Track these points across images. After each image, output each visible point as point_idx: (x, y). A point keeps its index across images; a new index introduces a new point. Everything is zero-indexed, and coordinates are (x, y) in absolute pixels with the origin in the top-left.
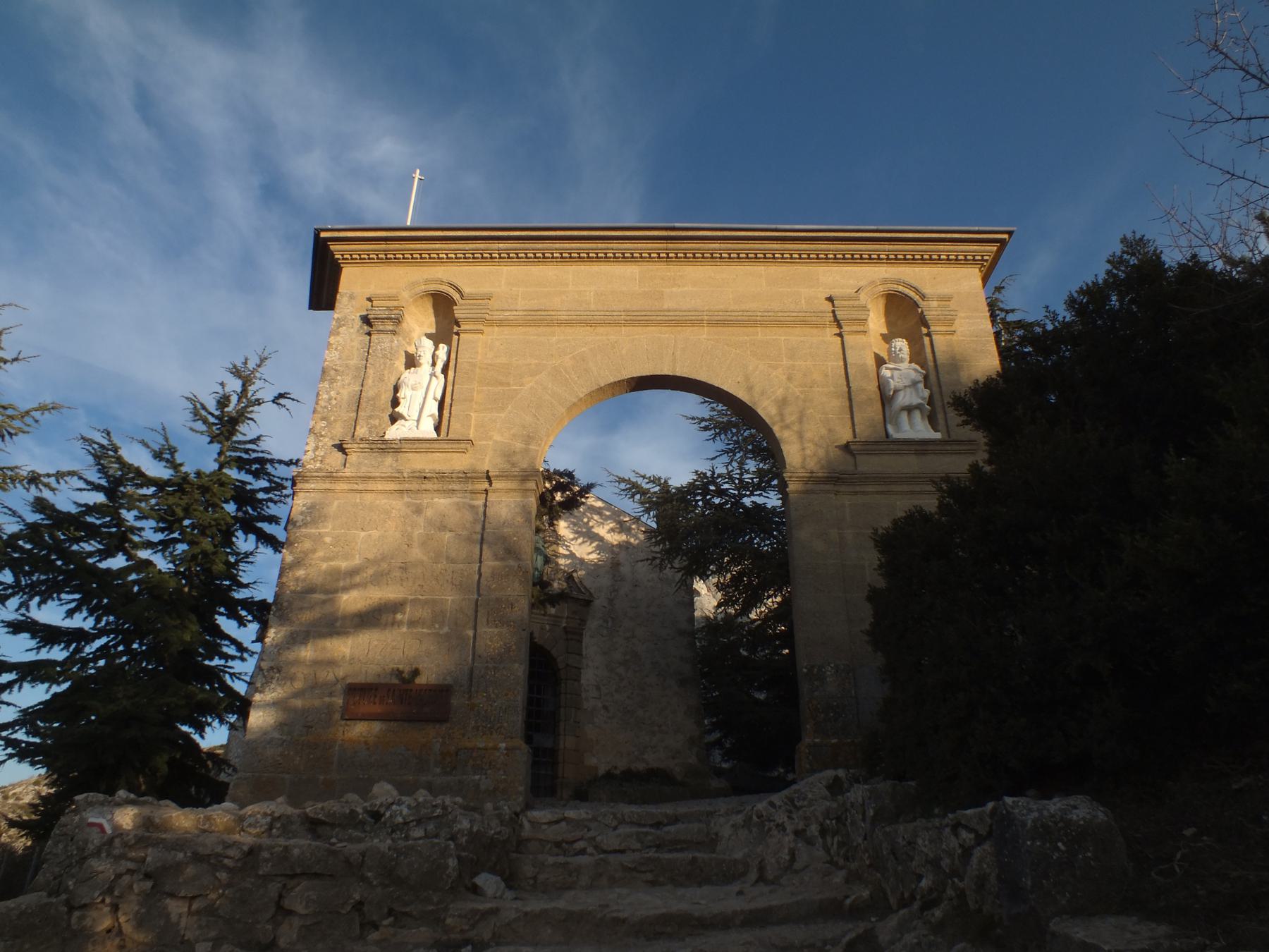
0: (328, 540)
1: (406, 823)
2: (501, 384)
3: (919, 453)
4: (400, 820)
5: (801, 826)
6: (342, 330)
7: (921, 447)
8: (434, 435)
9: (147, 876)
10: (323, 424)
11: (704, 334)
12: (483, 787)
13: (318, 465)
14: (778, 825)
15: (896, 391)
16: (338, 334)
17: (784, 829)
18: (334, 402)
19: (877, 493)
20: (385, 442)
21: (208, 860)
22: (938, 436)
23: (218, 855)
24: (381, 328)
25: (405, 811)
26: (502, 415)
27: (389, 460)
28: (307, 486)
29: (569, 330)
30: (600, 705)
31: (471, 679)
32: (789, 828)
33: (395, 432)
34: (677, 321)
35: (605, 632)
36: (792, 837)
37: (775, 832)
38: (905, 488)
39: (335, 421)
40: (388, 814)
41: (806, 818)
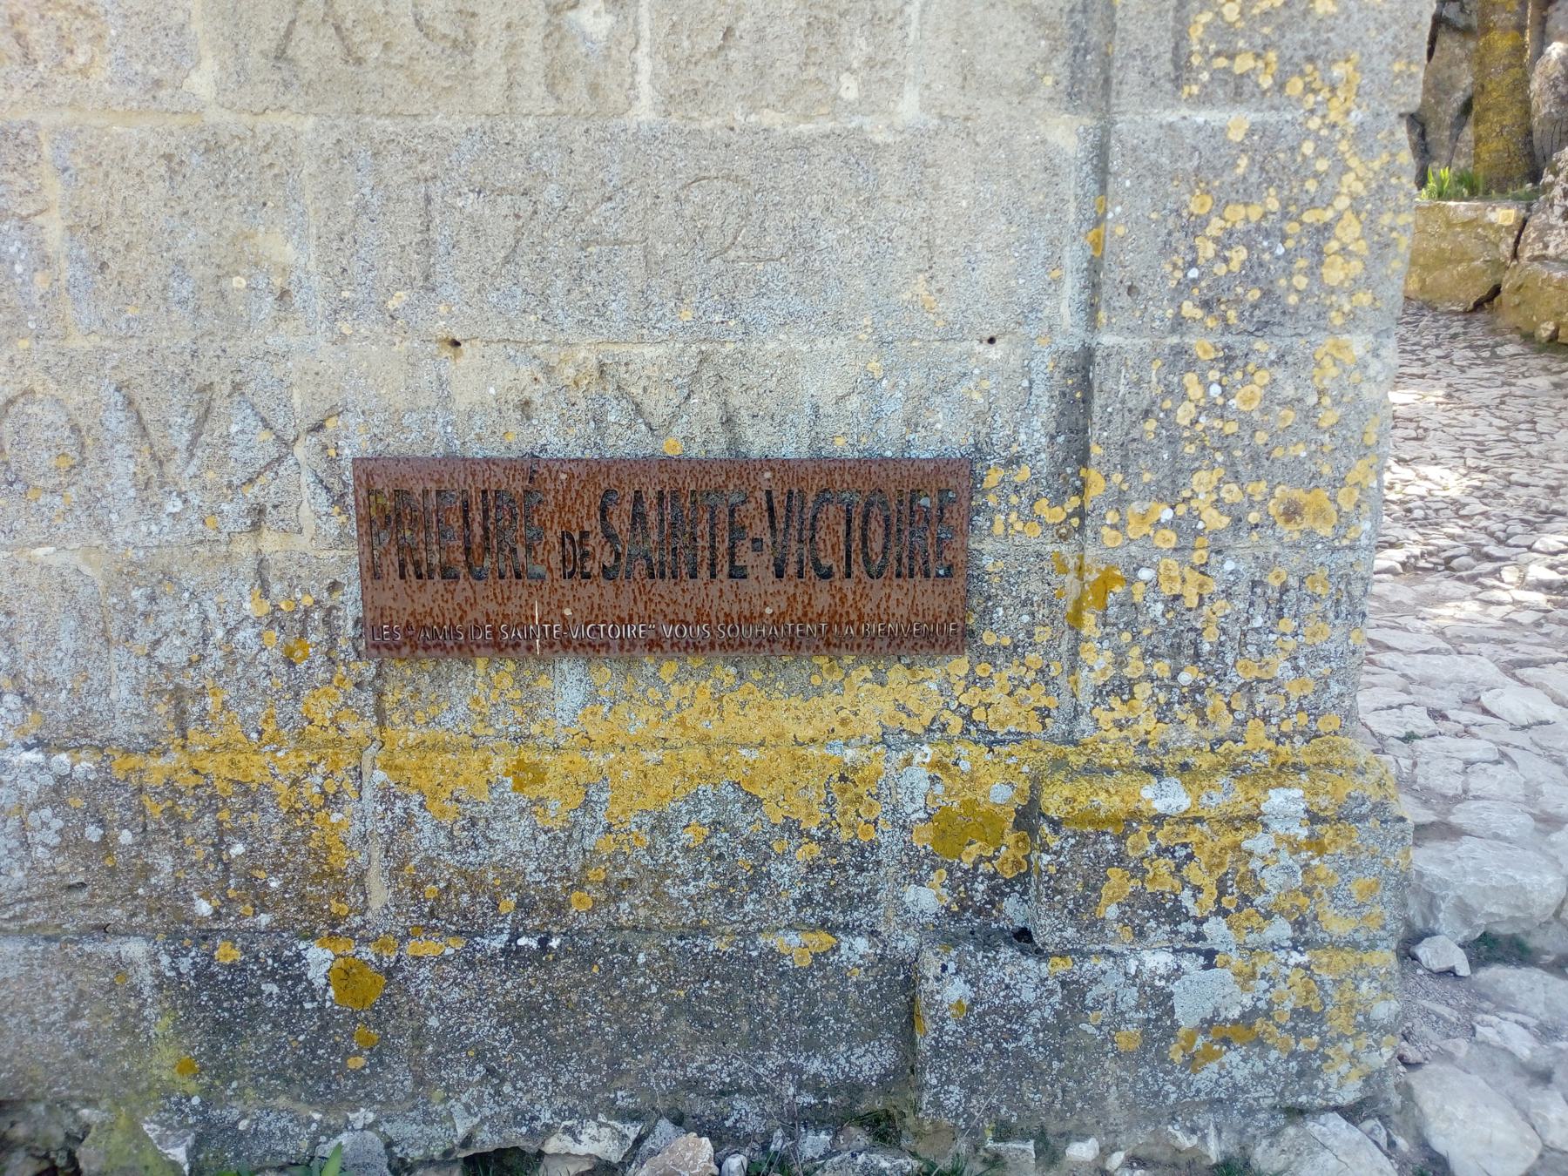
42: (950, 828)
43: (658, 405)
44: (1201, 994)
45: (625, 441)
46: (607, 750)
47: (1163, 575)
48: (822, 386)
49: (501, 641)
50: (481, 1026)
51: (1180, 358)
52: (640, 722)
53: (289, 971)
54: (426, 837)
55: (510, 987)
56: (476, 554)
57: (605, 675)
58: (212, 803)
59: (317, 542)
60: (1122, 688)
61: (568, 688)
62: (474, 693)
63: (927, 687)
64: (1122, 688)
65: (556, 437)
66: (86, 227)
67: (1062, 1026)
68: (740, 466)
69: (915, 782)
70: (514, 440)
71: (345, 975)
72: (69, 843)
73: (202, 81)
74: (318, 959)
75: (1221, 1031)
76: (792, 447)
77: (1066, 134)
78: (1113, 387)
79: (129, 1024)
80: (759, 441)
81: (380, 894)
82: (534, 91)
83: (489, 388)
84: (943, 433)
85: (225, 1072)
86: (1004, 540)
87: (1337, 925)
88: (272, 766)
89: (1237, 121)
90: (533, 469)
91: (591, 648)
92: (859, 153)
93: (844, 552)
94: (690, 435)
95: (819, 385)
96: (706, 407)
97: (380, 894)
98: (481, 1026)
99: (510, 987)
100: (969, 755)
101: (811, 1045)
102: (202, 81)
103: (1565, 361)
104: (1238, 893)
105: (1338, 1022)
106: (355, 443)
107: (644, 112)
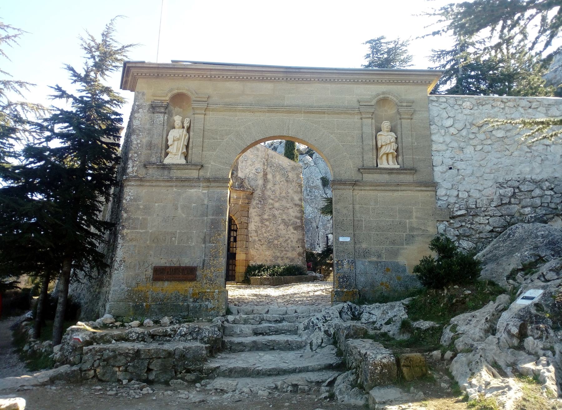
0: (141, 207)
1: (185, 334)
2: (214, 139)
3: (389, 174)
4: (184, 333)
5: (327, 329)
6: (140, 110)
7: (390, 171)
8: (183, 161)
9: (104, 360)
10: (136, 155)
11: (301, 118)
12: (209, 307)
13: (135, 174)
14: (319, 328)
15: (382, 146)
16: (139, 112)
17: (320, 330)
18: (140, 145)
19: (370, 190)
20: (164, 165)
21: (126, 355)
22: (398, 167)
23: (127, 353)
24: (158, 110)
25: (185, 329)
26: (215, 153)
27: (166, 172)
28: (129, 183)
29: (243, 114)
30: (257, 239)
31: (203, 264)
32: (322, 329)
33: (167, 161)
34: (292, 110)
35: (260, 206)
36: (323, 333)
37: (317, 330)
38: (383, 188)
39: (141, 154)
40: (179, 331)
41: (329, 325)
42: (193, 294)
43: (175, 263)
44: (210, 306)
45: (172, 265)
46: (168, 288)
47: (209, 275)
48: (186, 262)
49: (162, 280)
50: (156, 310)
51: (210, 260)
52: (171, 286)
53: (142, 305)
54: (154, 295)
55: (159, 306)
56: (161, 273)
57: (169, 282)
58: (139, 292)
59: (150, 272)
60: (206, 283)
61: (166, 284)
62: (159, 284)
63: (193, 284)
64: (206, 283)
65: (168, 265)
66: (138, 251)
67: (200, 308)
68: (180, 267)
69: (191, 291)
70: (165, 265)
71: (146, 306)
72: (128, 295)
73: (148, 242)
74: (145, 304)
75: (213, 309)
76: (184, 265)
77: (203, 246)
78: (206, 262)
79: (129, 309)
80: (182, 265)
81: (150, 299)
82: (169, 243)
83: (163, 262)
84: (195, 265)
85: (136, 314)
86: (199, 273)
87: (221, 301)
88: (144, 289)
89: (214, 245)
90: (166, 267)
91: (168, 280)
92: (190, 247)
93: (187, 273)
94: (177, 265)
95: (186, 261)
96: (178, 263)
97: (150, 299)
98: (156, 310)
99: (159, 306)
100: (195, 289)
101: (181, 312)
102: (148, 242)
103: (561, 21)
104: (213, 298)
105: (220, 308)
106: (154, 265)
107: (176, 244)
